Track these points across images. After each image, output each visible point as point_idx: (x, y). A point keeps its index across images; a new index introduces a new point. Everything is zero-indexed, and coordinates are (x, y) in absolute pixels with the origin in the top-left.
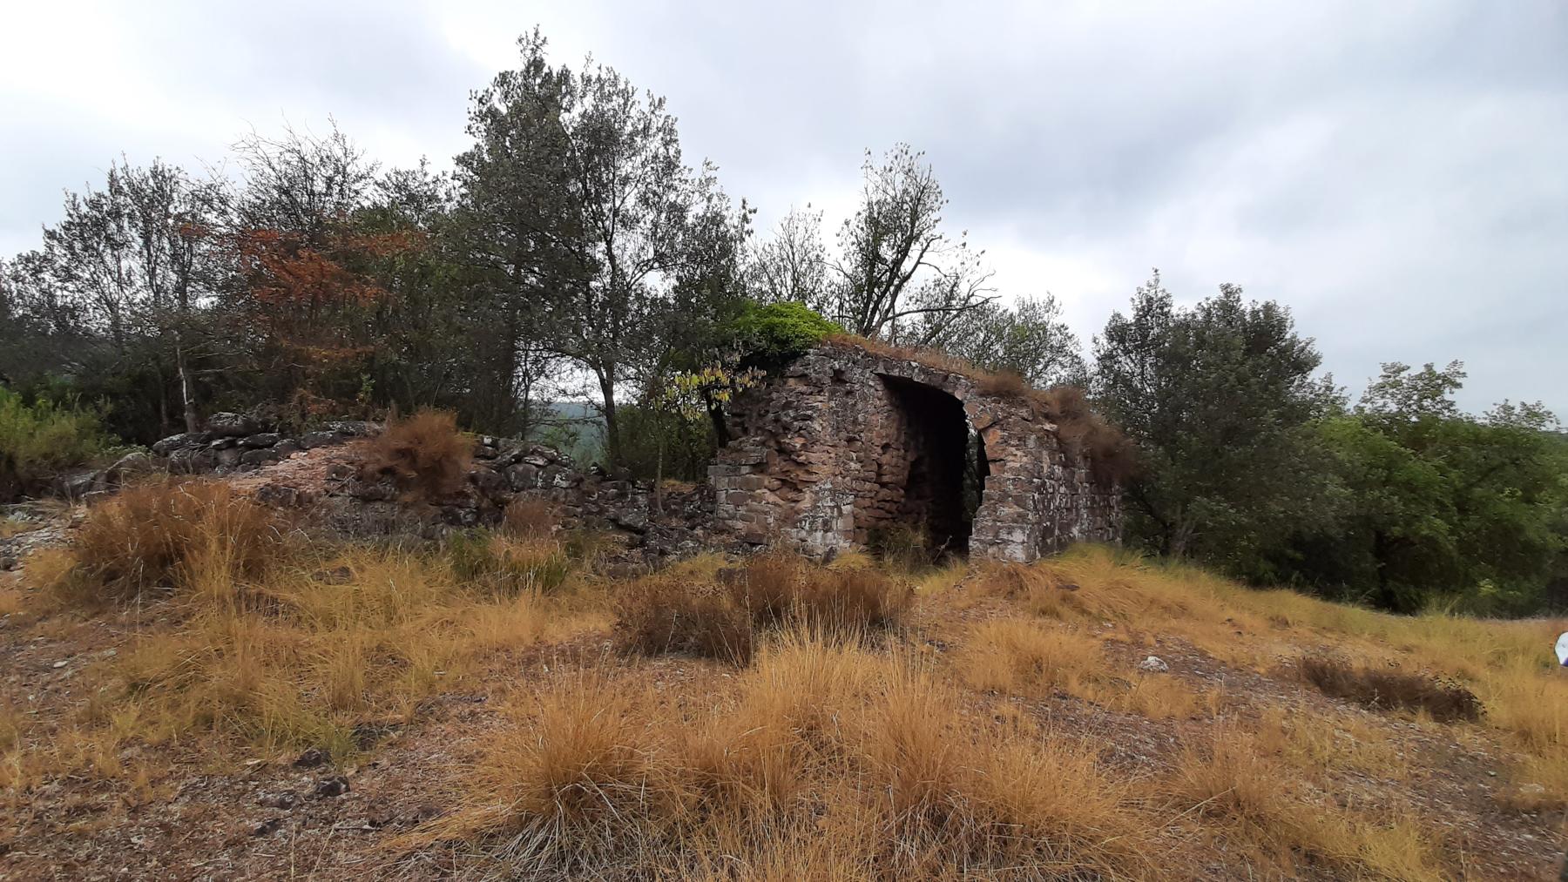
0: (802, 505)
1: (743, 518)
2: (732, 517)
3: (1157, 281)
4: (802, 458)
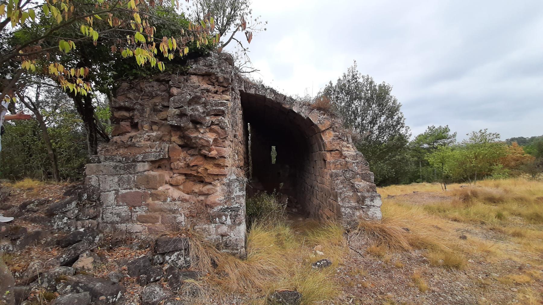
0: (211, 199)
1: (142, 220)
2: (128, 220)
3: (356, 66)
4: (214, 153)
